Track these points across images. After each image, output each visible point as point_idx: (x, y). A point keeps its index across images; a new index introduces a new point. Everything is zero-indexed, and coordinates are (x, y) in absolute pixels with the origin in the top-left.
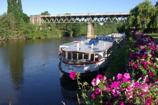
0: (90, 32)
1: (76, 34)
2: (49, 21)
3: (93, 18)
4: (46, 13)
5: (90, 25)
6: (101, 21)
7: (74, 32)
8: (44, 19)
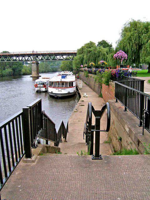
3: (37, 57)
6: (40, 59)
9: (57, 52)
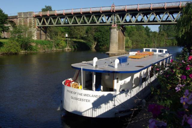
0: (116, 43)
1: (101, 47)
2: (88, 22)
4: (49, 9)
5: (115, 30)
6: (151, 20)
7: (98, 42)
8: (39, 19)
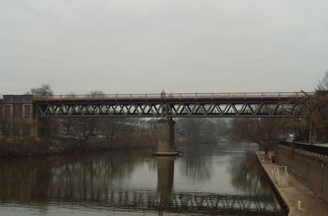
3: (172, 106)
6: (179, 112)
9: (220, 96)
